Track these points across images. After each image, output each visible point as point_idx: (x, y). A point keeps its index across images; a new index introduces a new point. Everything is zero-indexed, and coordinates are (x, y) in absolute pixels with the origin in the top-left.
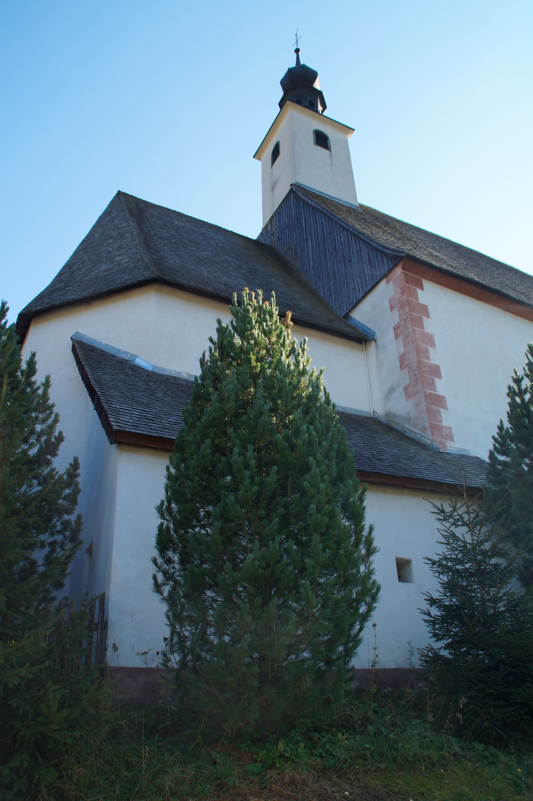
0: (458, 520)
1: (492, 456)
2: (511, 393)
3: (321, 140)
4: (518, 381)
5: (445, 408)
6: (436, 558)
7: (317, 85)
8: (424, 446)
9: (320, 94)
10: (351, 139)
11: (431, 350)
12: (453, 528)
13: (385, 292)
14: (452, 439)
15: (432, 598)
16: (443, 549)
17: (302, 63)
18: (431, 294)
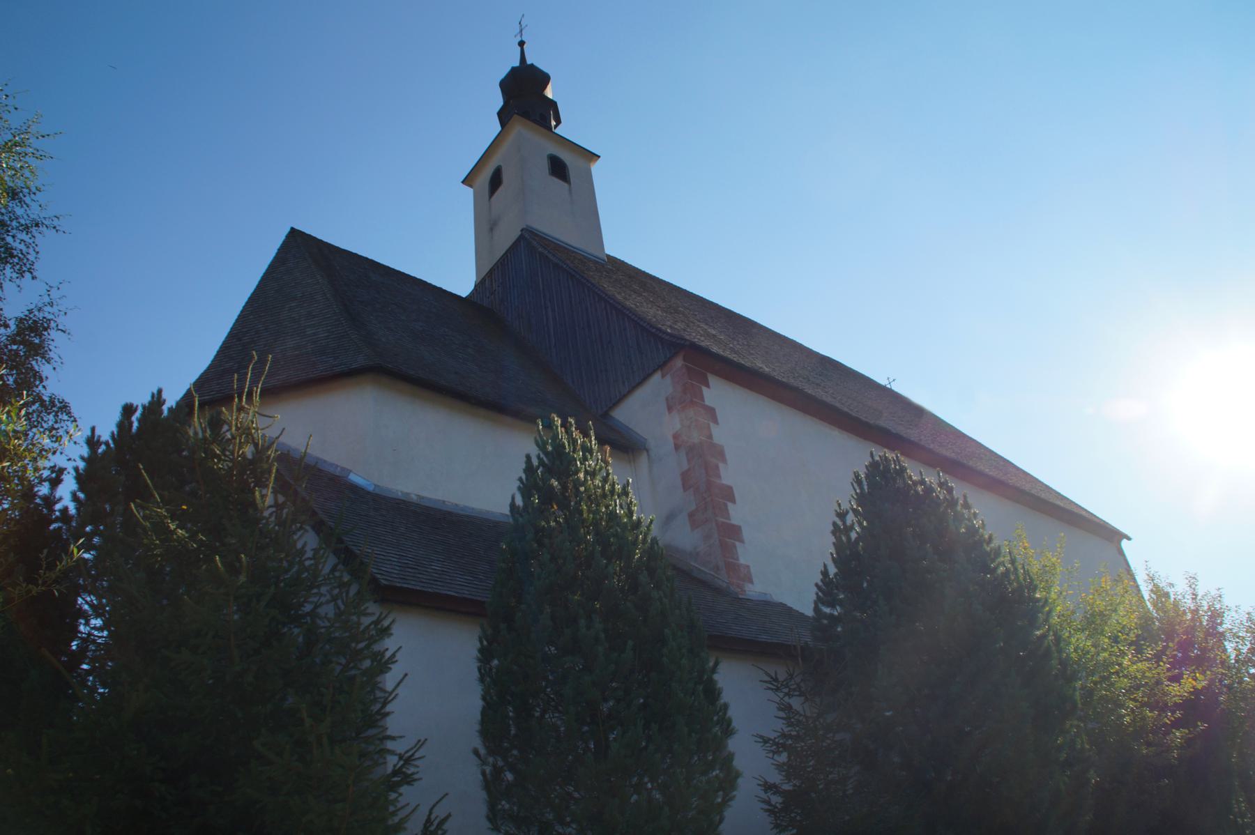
0: (794, 690)
1: (816, 609)
2: (836, 531)
3: (558, 169)
4: (842, 515)
5: (742, 541)
6: (772, 735)
7: (549, 93)
8: (718, 591)
9: (553, 105)
10: (596, 168)
11: (721, 465)
12: (786, 699)
13: (658, 387)
14: (751, 582)
15: (766, 782)
16: (780, 725)
17: (529, 62)
18: (718, 393)
